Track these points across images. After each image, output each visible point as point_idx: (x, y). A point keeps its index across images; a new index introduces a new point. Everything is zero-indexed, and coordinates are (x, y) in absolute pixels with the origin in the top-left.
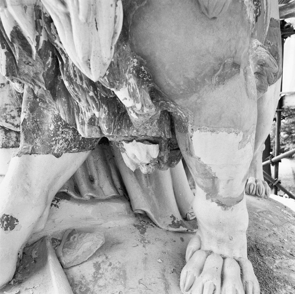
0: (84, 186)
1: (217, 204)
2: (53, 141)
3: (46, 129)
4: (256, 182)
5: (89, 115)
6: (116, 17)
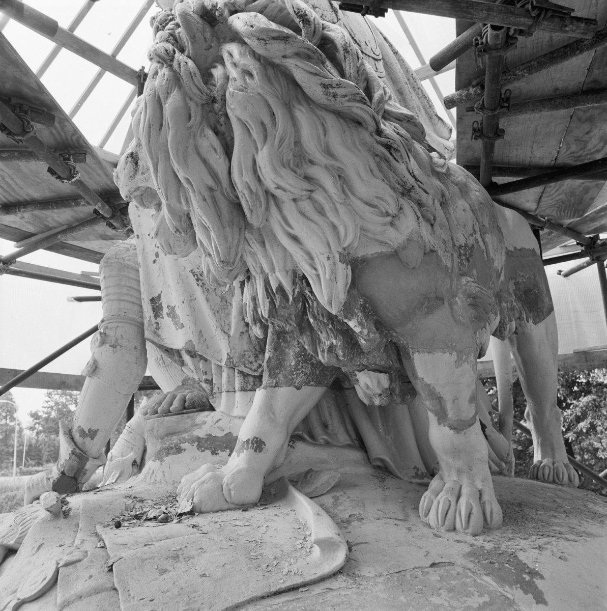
0: (318, 430)
1: (448, 429)
2: (294, 375)
3: (288, 364)
4: (553, 464)
5: (328, 343)
6: (347, 274)
